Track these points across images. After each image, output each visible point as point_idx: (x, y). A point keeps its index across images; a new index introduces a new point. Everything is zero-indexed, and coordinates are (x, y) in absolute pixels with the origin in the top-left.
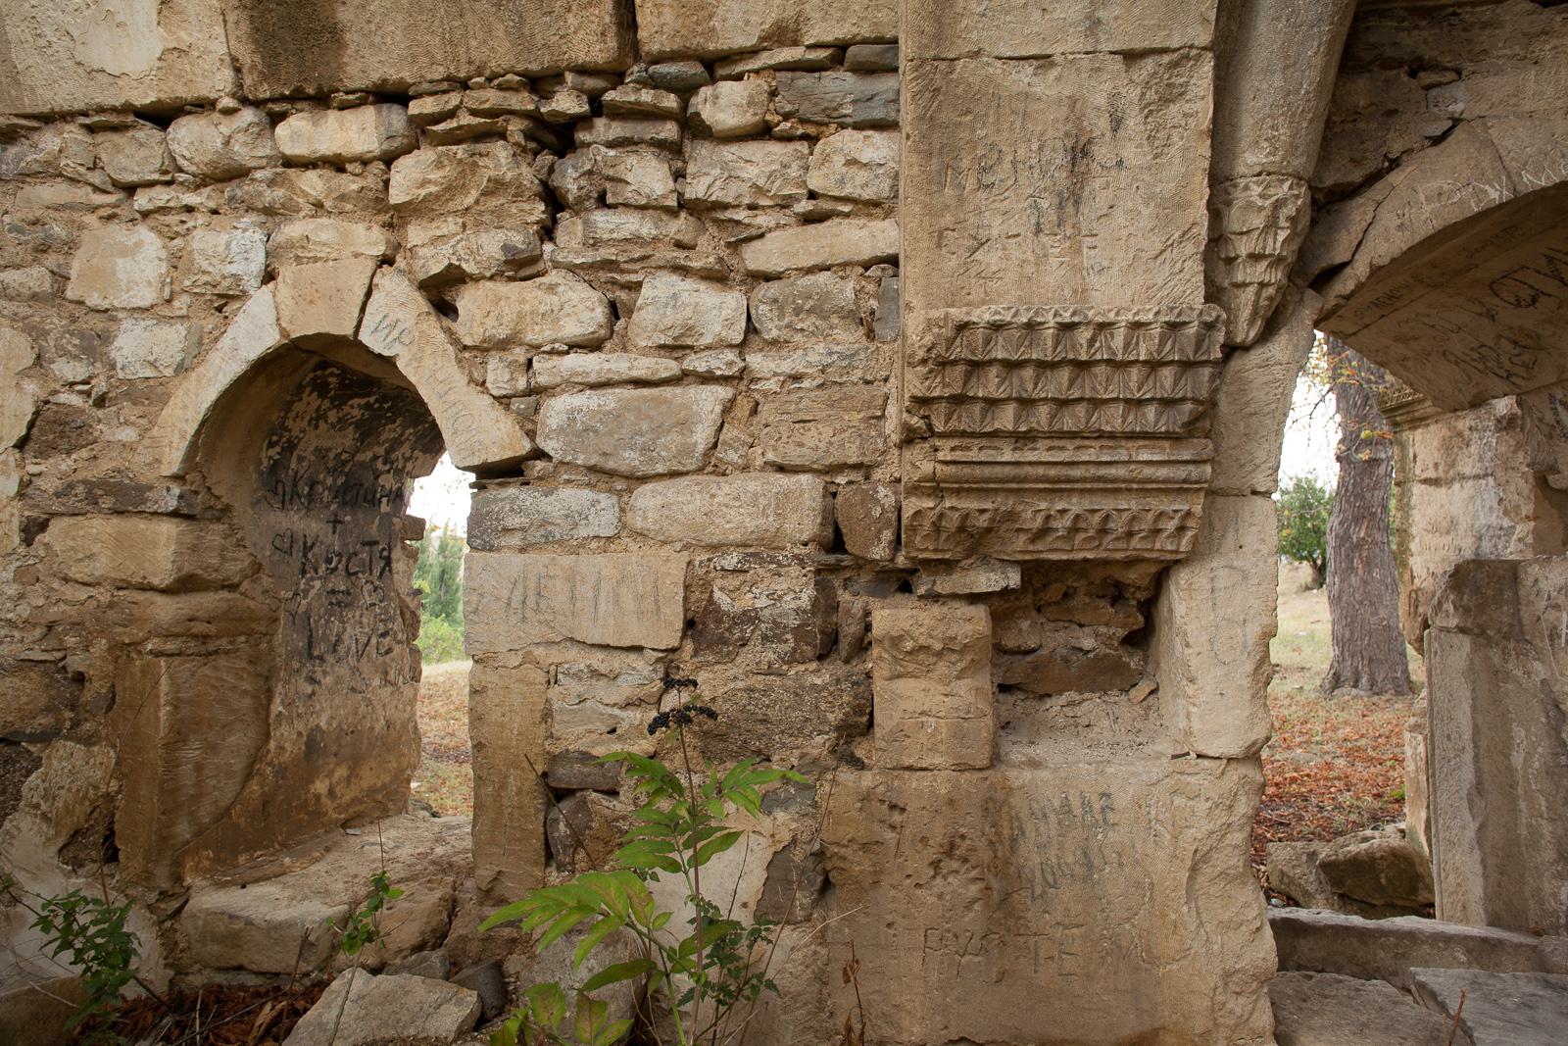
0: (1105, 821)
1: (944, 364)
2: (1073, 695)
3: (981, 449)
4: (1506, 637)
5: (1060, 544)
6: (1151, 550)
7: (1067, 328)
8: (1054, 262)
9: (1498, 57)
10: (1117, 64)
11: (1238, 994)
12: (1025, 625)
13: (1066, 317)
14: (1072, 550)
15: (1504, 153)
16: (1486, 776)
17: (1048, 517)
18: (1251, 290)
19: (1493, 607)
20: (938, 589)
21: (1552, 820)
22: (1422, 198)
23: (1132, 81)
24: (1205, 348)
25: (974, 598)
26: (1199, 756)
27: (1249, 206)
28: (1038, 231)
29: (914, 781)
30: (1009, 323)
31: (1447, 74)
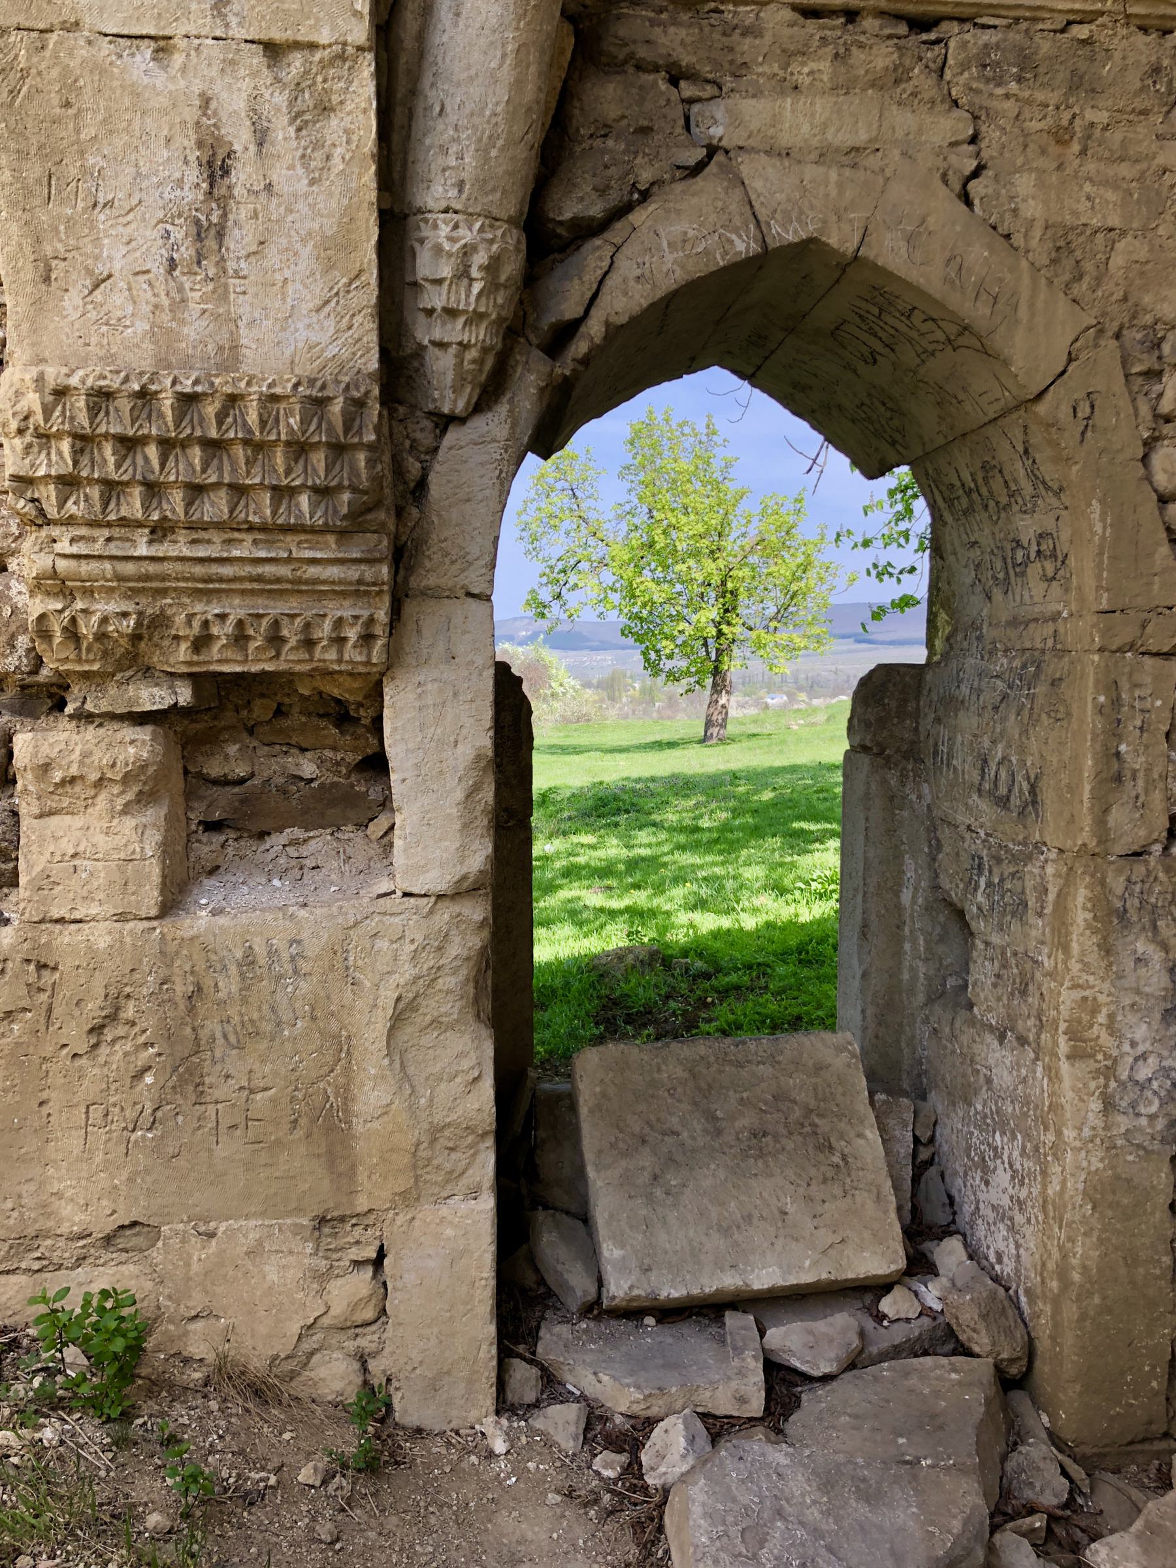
0: (296, 972)
1: (45, 438)
2: (298, 833)
3: (109, 540)
4: (906, 756)
5: (229, 654)
6: (209, 663)
7: (187, 401)
8: (195, 308)
9: (759, 74)
10: (255, 58)
11: (452, 1149)
12: (232, 749)
13: (187, 386)
14: (246, 661)
15: (753, 197)
16: (873, 917)
17: (206, 624)
18: (453, 350)
19: (895, 720)
20: (89, 707)
21: (927, 960)
22: (665, 244)
23: (278, 80)
24: (356, 428)
25: (140, 719)
26: (406, 895)
27: (438, 250)
28: (172, 264)
29: (67, 936)
30: (119, 391)
31: (708, 87)
